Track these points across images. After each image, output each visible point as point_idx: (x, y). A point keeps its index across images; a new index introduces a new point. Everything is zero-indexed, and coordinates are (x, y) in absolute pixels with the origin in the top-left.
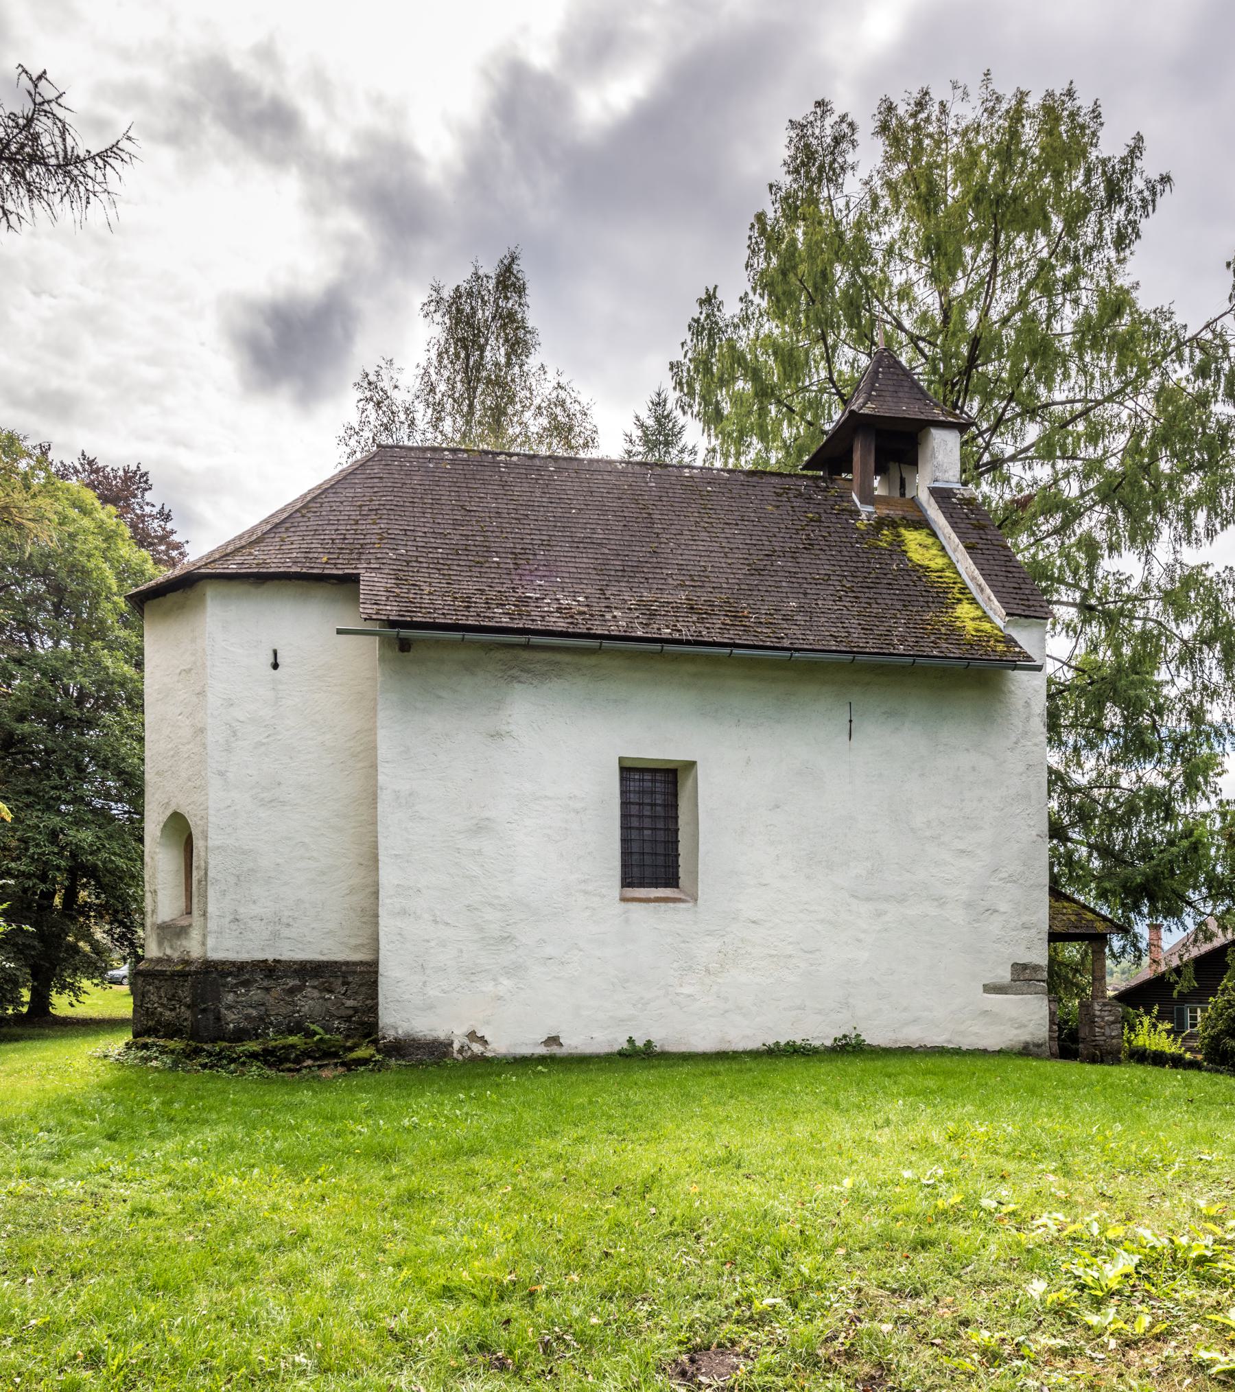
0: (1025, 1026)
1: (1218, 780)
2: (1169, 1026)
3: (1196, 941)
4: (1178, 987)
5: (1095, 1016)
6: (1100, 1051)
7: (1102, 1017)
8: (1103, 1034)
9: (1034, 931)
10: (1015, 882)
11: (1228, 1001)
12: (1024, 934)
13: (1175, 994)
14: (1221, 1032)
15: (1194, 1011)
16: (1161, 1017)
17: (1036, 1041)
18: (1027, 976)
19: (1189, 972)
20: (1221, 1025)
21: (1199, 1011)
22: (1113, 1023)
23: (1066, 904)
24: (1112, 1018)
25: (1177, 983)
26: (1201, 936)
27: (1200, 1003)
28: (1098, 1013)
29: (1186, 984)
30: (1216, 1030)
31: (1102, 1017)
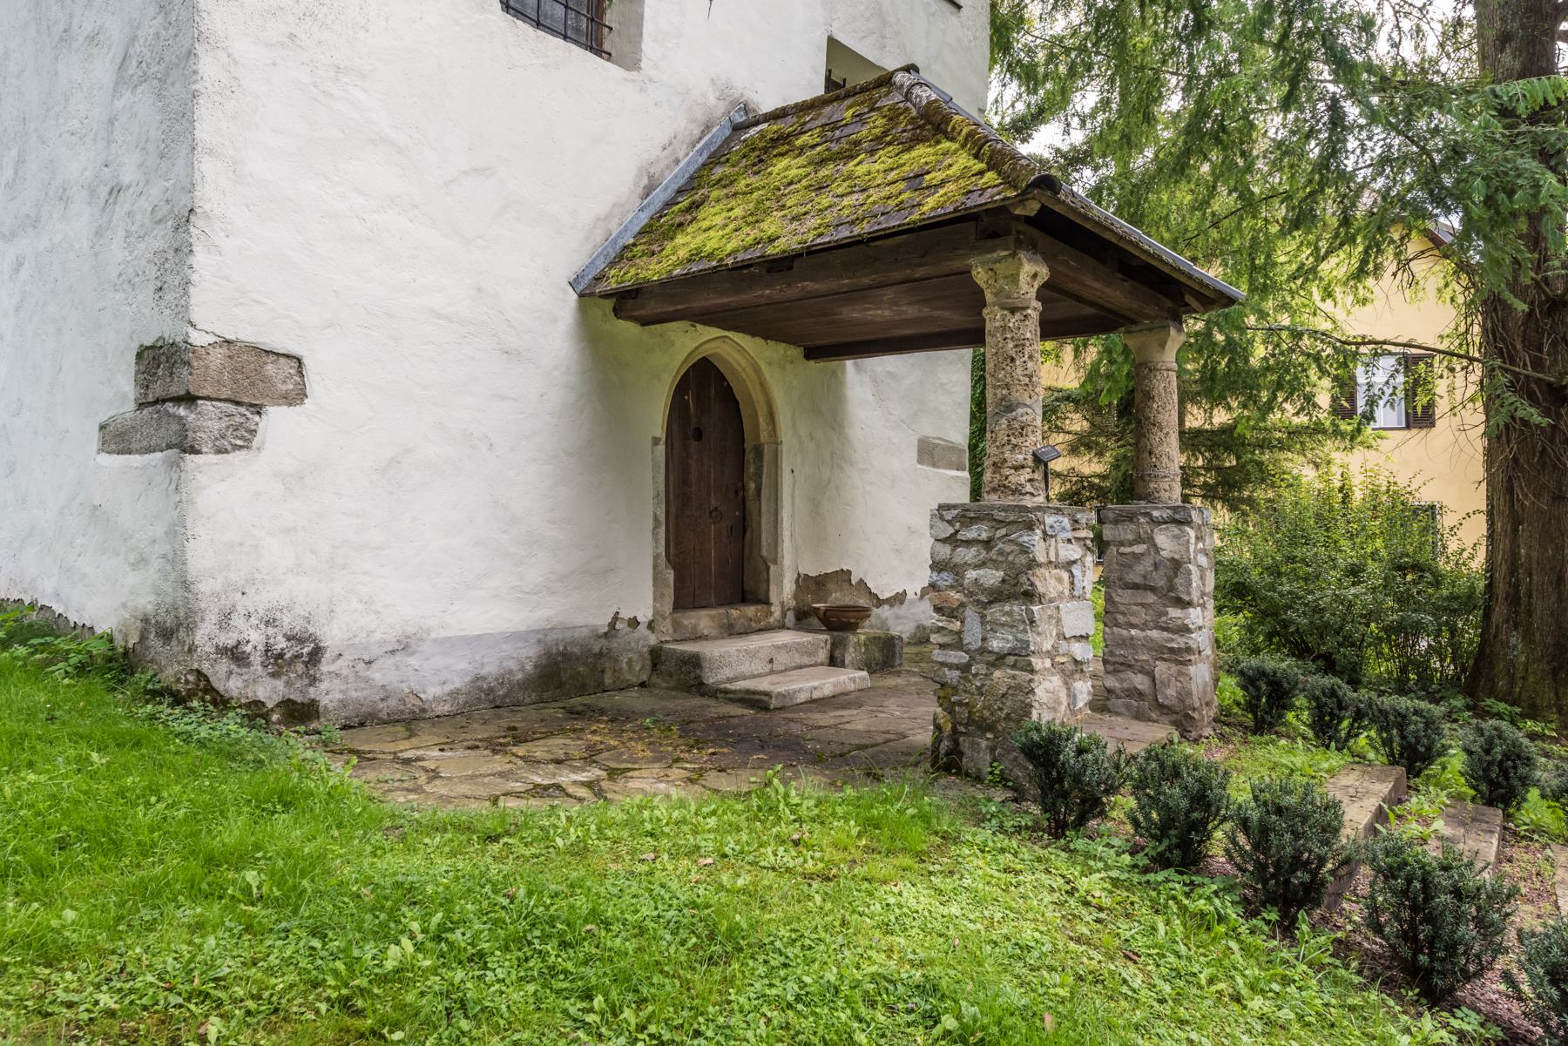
8: (959, 645)
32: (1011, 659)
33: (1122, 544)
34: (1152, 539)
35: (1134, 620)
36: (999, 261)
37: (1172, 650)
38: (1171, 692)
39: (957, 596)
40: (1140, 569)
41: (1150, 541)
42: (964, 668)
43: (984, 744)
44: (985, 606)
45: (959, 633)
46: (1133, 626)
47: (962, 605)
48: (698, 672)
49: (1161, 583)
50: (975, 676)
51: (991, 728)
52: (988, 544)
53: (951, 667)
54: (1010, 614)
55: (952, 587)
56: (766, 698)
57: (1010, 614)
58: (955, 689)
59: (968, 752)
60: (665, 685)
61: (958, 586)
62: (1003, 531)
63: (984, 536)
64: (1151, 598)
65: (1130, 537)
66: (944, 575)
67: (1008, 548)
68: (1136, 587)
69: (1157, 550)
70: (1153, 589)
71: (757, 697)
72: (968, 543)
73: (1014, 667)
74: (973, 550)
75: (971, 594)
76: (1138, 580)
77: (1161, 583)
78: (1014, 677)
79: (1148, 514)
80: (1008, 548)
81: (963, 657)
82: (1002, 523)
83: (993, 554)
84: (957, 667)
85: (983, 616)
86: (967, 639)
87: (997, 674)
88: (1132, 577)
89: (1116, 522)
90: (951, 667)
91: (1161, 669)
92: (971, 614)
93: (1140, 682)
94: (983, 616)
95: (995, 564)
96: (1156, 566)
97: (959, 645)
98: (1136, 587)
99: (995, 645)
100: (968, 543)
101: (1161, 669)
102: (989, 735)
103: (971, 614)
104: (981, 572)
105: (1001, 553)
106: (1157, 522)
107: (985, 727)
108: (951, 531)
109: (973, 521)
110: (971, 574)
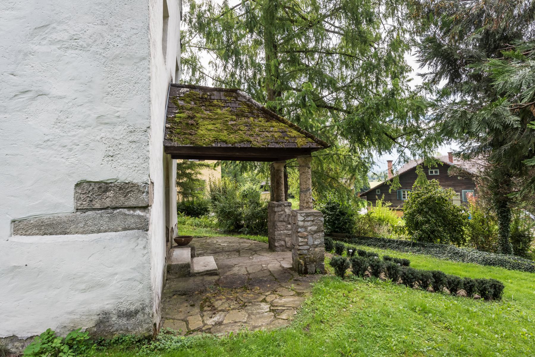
0: (101, 285)
1: (409, 83)
2: (390, 204)
3: (399, 162)
4: (391, 188)
5: (299, 227)
6: (304, 260)
7: (305, 228)
8: (307, 244)
9: (120, 130)
10: (82, 48)
11: (418, 194)
12: (104, 132)
13: (390, 191)
14: (414, 211)
15: (404, 192)
16: (386, 200)
17: (124, 308)
18: (108, 202)
19: (398, 180)
20: (414, 207)
21: (406, 192)
22: (316, 232)
23: (274, 124)
24: (314, 228)
25: (390, 185)
26: (402, 160)
27: (406, 189)
28: (301, 224)
29: (395, 185)
30: (412, 210)
31: (305, 228)
32: (320, 245)
33: (279, 212)
34: (284, 210)
35: (281, 229)
36: (308, 157)
37: (289, 234)
38: (289, 244)
39: (306, 233)
40: (282, 217)
41: (284, 210)
42: (308, 250)
43: (313, 265)
44: (313, 235)
45: (307, 242)
46: (281, 230)
47: (308, 235)
48: (189, 269)
49: (286, 220)
50: (311, 251)
51: (315, 261)
52: (313, 221)
53: (305, 250)
54: (319, 236)
55: (304, 231)
56: (216, 271)
57: (319, 236)
58: (306, 255)
59: (309, 268)
60: (174, 277)
61: (306, 231)
62: (317, 218)
63: (312, 219)
64: (284, 223)
65: (280, 210)
66: (302, 229)
67: (318, 221)
68: (281, 221)
69: (285, 212)
70: (285, 221)
71: (212, 272)
72: (308, 221)
73: (320, 247)
74: (310, 223)
75: (309, 232)
76: (282, 220)
77: (286, 220)
78: (320, 249)
79: (284, 205)
80: (318, 221)
81: (308, 247)
82: (316, 216)
83: (314, 223)
84: (306, 250)
85: (313, 237)
86: (309, 243)
87: (316, 249)
88: (281, 219)
89: (277, 207)
90: (305, 250)
91: (287, 239)
92: (310, 237)
93: (283, 243)
94: (313, 237)
95: (315, 225)
96: (286, 216)
97: (307, 244)
98: (281, 221)
99: (316, 243)
100: (308, 221)
101: (287, 239)
102: (315, 263)
103: (310, 237)
104: (312, 227)
105: (316, 222)
106: (285, 206)
107: (313, 261)
108: (304, 218)
109: (309, 216)
110: (309, 228)
